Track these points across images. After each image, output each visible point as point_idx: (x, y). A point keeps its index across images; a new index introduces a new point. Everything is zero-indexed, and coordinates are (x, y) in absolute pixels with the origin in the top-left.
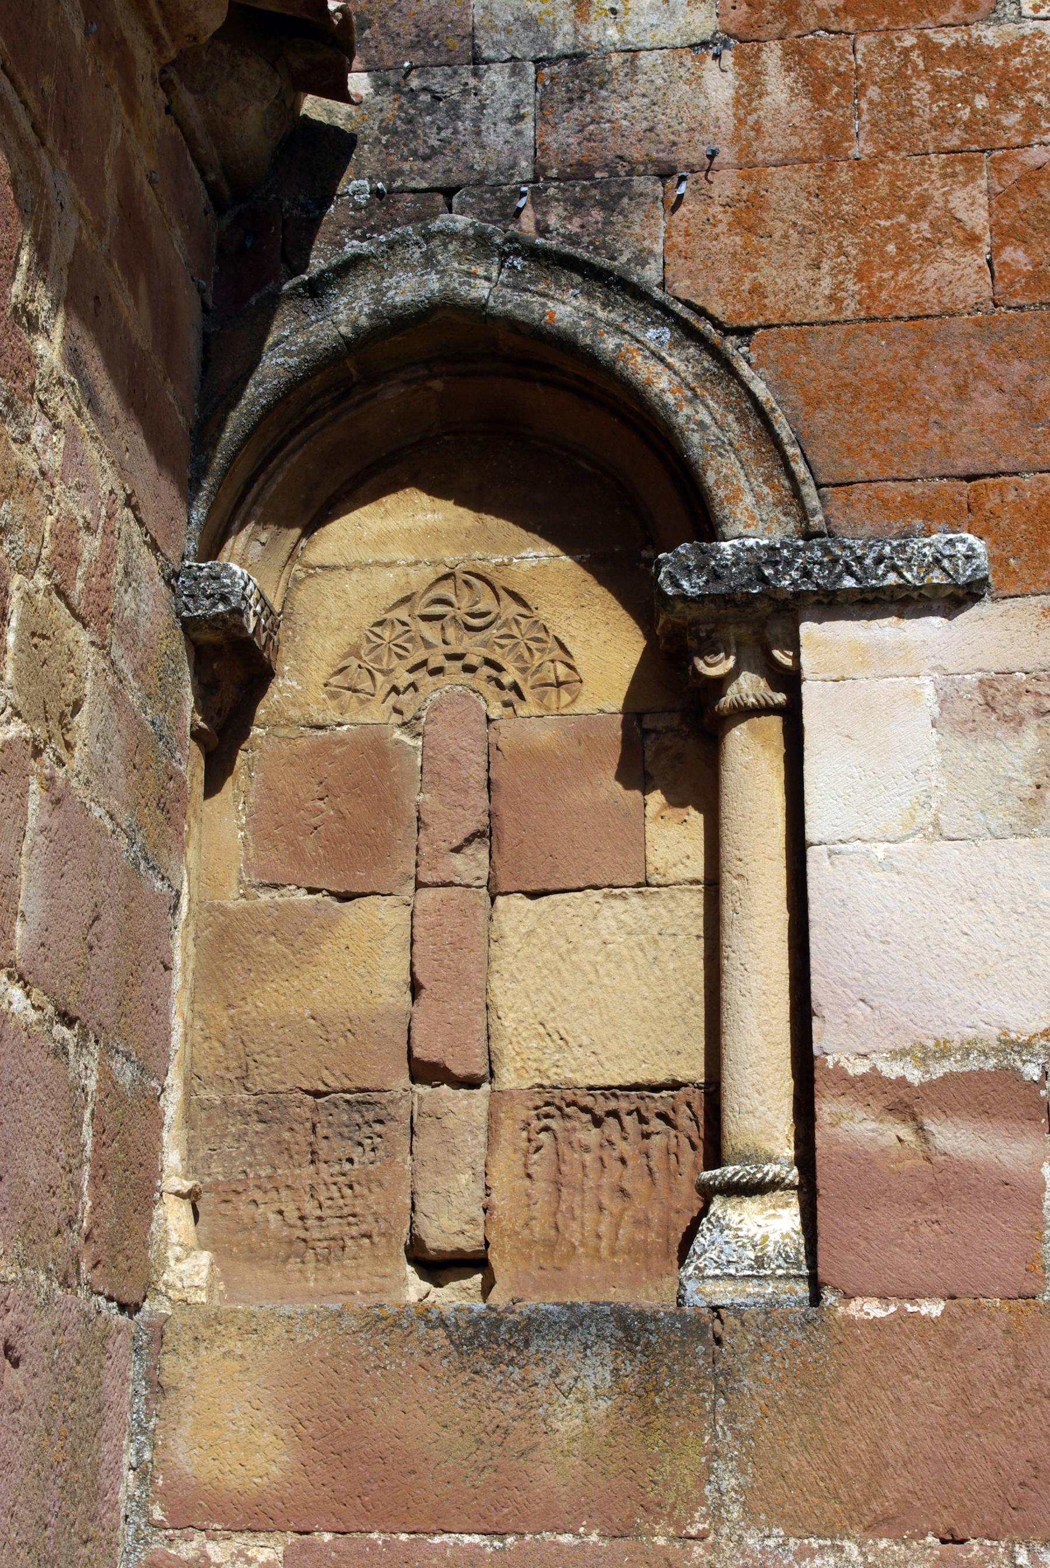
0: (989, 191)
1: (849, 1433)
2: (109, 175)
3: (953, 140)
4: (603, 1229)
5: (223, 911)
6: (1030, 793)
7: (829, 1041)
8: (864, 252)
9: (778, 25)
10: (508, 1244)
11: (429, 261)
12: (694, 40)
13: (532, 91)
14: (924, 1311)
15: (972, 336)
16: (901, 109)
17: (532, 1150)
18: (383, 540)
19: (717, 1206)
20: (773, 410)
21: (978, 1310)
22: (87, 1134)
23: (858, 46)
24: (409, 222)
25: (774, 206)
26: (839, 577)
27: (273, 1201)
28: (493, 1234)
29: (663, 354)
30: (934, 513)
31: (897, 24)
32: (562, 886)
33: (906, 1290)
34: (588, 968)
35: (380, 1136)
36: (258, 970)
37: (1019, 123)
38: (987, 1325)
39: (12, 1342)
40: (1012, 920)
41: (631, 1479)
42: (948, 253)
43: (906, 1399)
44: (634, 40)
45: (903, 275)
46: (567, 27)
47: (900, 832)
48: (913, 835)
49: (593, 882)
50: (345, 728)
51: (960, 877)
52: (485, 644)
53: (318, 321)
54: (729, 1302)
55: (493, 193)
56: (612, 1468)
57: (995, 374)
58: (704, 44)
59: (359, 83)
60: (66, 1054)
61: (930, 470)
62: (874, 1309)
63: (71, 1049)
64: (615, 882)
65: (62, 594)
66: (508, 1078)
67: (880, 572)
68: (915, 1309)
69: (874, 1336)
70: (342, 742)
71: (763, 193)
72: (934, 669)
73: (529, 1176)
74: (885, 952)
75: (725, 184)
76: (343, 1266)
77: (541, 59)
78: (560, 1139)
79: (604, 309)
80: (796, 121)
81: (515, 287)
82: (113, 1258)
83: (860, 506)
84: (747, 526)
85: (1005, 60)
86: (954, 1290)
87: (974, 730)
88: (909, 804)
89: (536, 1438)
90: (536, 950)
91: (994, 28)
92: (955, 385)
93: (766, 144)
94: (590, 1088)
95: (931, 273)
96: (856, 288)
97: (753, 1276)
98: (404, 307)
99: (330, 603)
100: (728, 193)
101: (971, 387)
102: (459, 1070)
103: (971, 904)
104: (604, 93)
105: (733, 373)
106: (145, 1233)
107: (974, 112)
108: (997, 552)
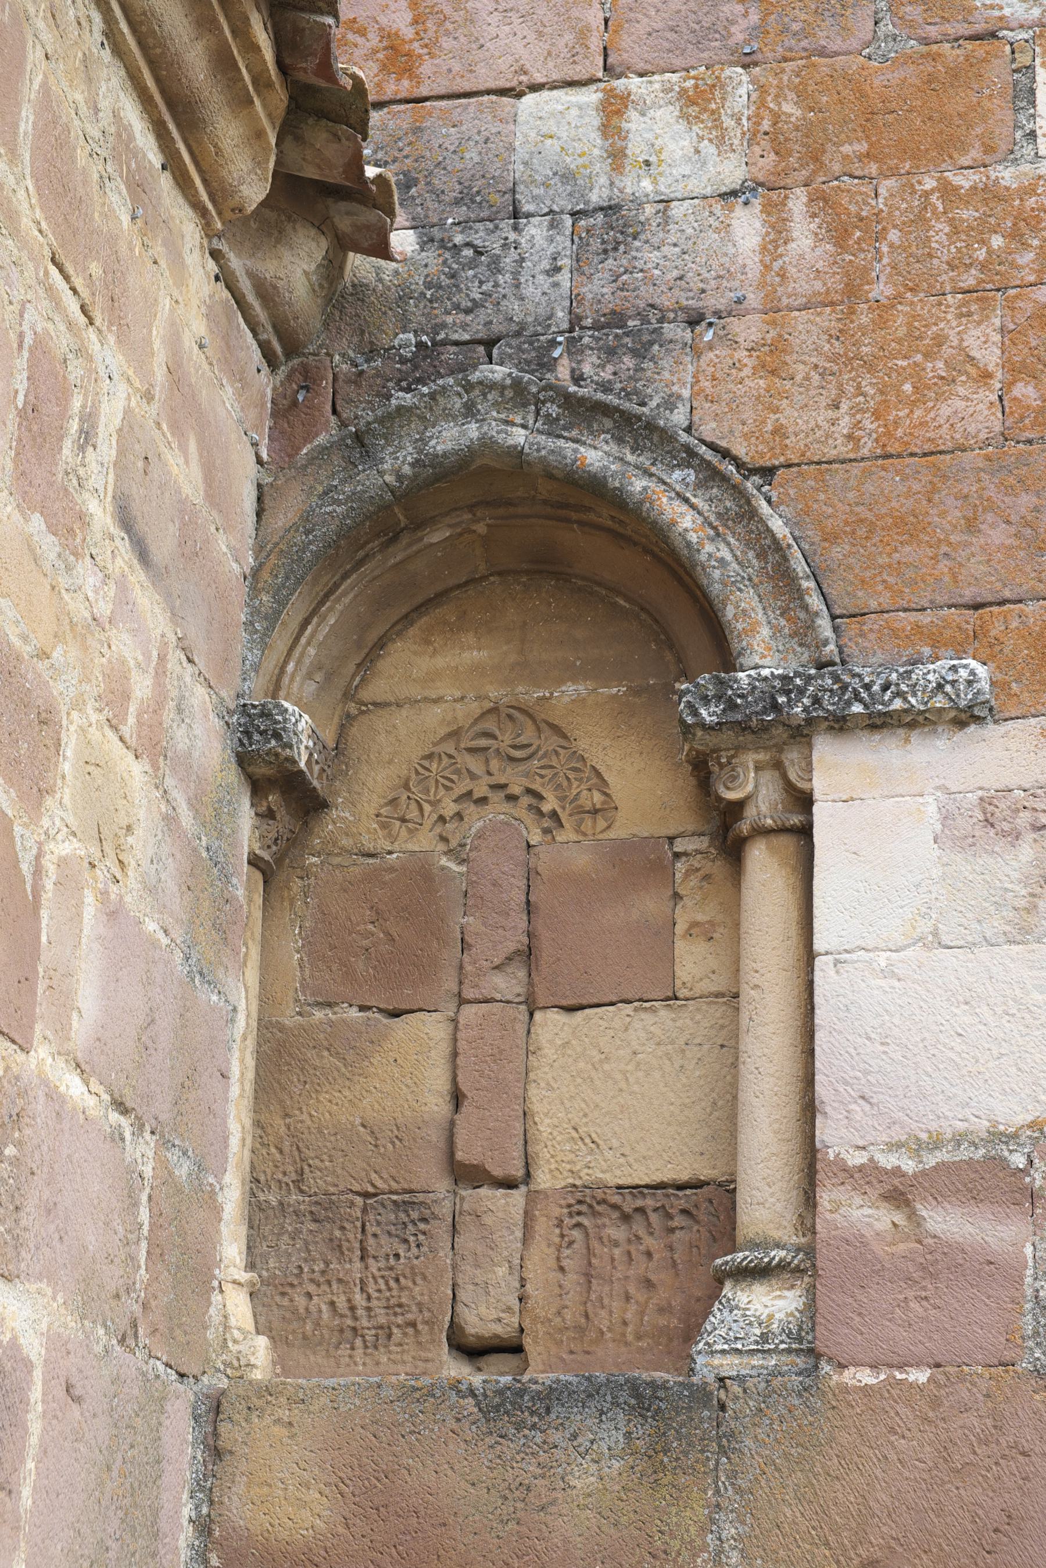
0: (1002, 330)
1: (839, 1487)
2: (157, 345)
3: (969, 280)
4: (629, 1316)
5: (282, 1028)
6: (1023, 903)
7: (833, 1135)
8: (882, 393)
9: (804, 172)
10: (541, 1329)
11: (470, 411)
12: (724, 189)
13: (568, 243)
14: (911, 1378)
15: (982, 470)
16: (920, 252)
17: (564, 1245)
18: (432, 677)
19: (728, 1290)
20: (789, 546)
21: (962, 1378)
22: (144, 1215)
23: (880, 191)
24: (452, 373)
25: (797, 349)
26: (849, 704)
27: (325, 1293)
28: (528, 1321)
29: (688, 495)
30: (940, 642)
31: (918, 167)
32: (596, 1001)
33: (896, 1360)
34: (619, 1076)
35: (424, 1233)
36: (312, 1082)
37: (1033, 262)
38: (969, 1390)
39: (73, 1381)
40: (1004, 1021)
41: (640, 1529)
42: (961, 391)
43: (893, 1456)
44: (667, 191)
45: (918, 413)
46: (603, 180)
47: (901, 941)
48: (914, 944)
49: (625, 996)
50: (395, 856)
51: (956, 982)
52: (527, 775)
53: (364, 470)
54: (735, 1373)
55: (531, 344)
56: (624, 1520)
57: (1003, 506)
58: (734, 193)
59: (403, 240)
60: (123, 1139)
61: (939, 599)
62: (866, 1377)
63: (128, 1135)
64: (645, 997)
65: (115, 728)
66: (543, 1179)
67: (886, 698)
68: (904, 1376)
69: (865, 1401)
70: (392, 869)
71: (787, 336)
72: (937, 788)
73: (562, 1269)
74: (885, 1053)
75: (749, 329)
76: (390, 1352)
77: (578, 212)
78: (591, 1235)
79: (633, 453)
80: (820, 265)
81: (549, 434)
82: (171, 1330)
83: (872, 636)
84: (763, 657)
85: (1022, 200)
86: (939, 1359)
87: (974, 845)
88: (910, 916)
89: (555, 1494)
90: (570, 1060)
91: (1012, 169)
92: (964, 517)
93: (790, 290)
94: (619, 1187)
95: (945, 410)
96: (873, 426)
97: (758, 1351)
98: (445, 454)
99: (382, 738)
100: (752, 337)
101: (981, 519)
102: (497, 1172)
103: (967, 1007)
104: (637, 243)
105: (751, 514)
106: (204, 1314)
107: (990, 252)
108: (999, 676)
